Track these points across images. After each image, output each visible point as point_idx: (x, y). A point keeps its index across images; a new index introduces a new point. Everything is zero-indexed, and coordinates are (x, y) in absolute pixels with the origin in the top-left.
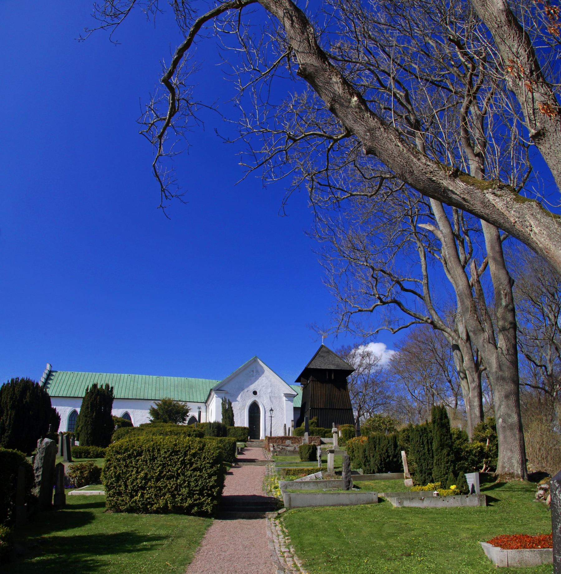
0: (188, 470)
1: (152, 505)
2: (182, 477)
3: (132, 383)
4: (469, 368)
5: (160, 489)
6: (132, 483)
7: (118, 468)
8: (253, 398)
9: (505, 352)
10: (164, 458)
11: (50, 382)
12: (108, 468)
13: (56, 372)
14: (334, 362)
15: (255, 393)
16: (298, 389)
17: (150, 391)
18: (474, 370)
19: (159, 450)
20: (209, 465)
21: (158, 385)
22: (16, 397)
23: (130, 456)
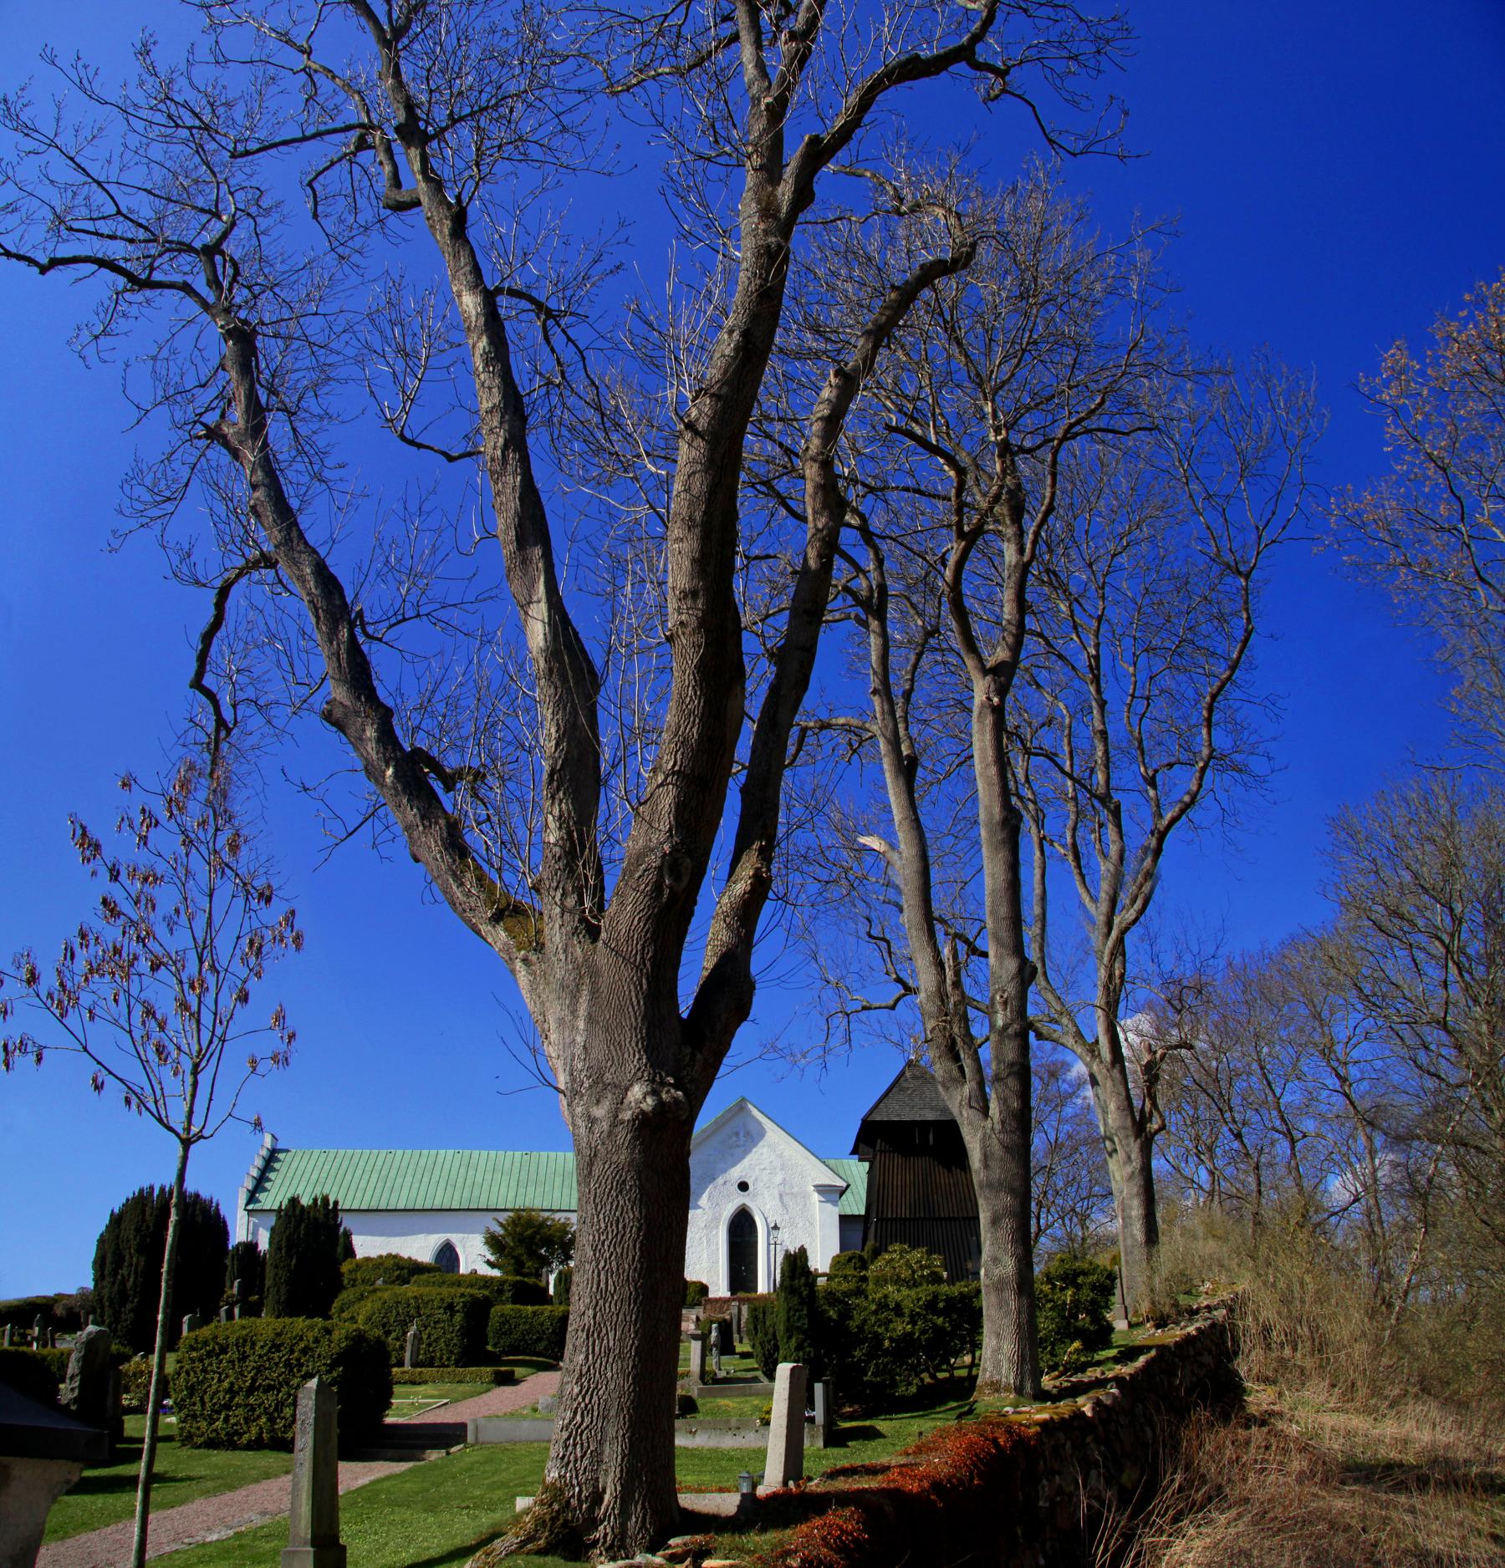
0: (294, 1376)
1: (241, 1435)
2: (284, 1389)
3: (463, 1170)
4: (1119, 1128)
5: (253, 1409)
6: (212, 1399)
7: (192, 1374)
8: (739, 1199)
9: (998, 1127)
10: (260, 1356)
11: (272, 1175)
12: (179, 1374)
13: (287, 1151)
14: (934, 1103)
15: (743, 1186)
16: (858, 1171)
17: (503, 1190)
18: (1130, 1133)
19: (253, 1344)
20: (323, 1368)
21: (524, 1174)
22: (148, 1228)
23: (209, 1354)
